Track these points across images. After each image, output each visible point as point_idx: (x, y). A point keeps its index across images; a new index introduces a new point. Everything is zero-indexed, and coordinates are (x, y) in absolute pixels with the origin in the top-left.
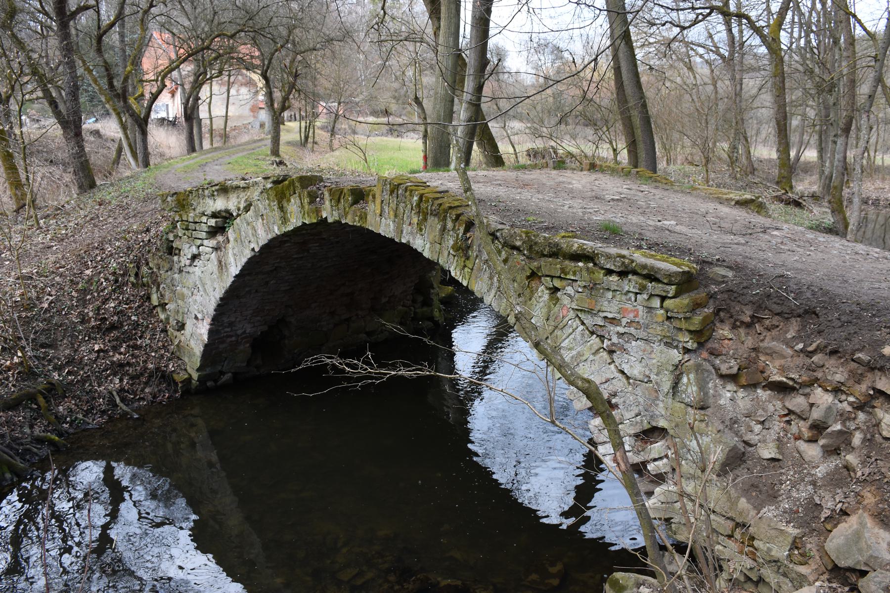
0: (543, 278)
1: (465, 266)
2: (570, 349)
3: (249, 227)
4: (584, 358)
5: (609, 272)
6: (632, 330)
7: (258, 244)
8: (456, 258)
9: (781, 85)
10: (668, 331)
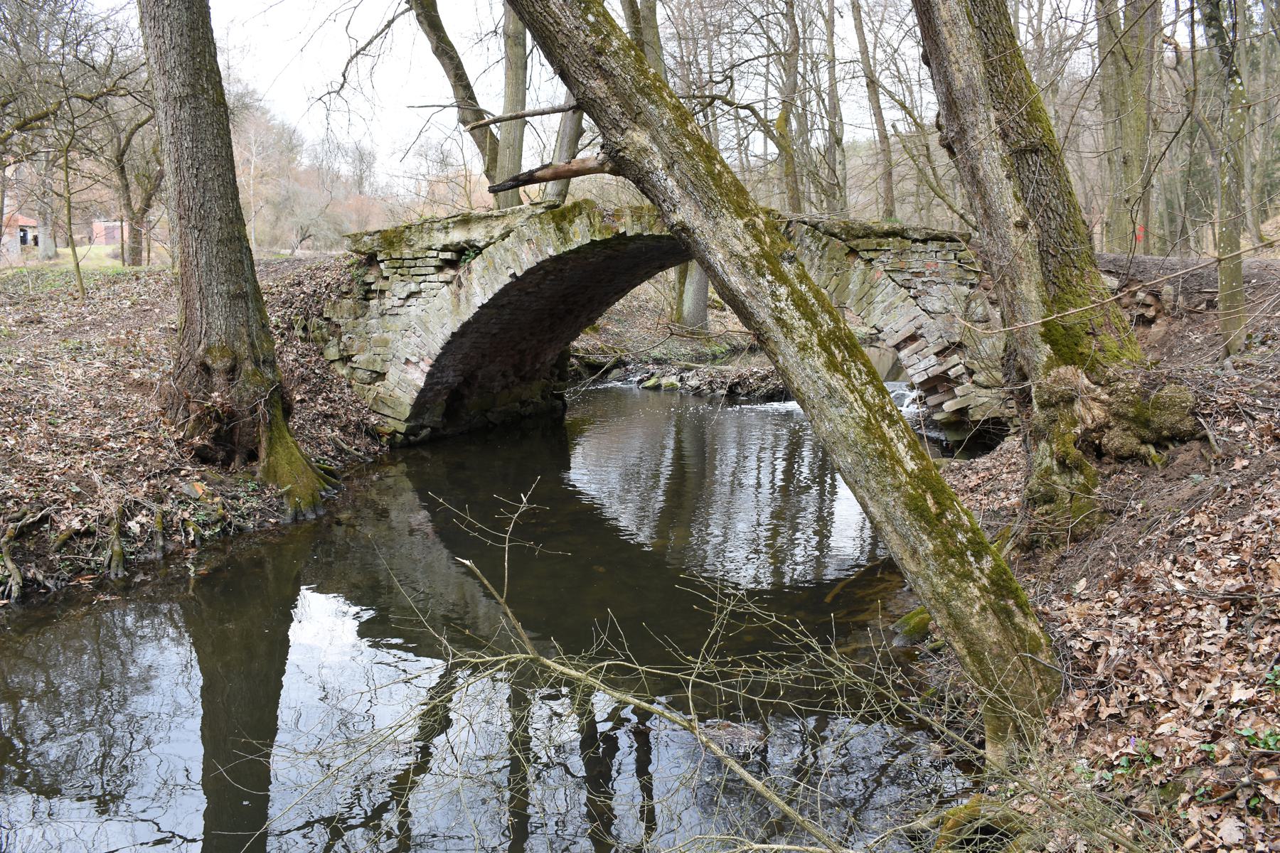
3: (508, 254)
5: (915, 241)
6: (934, 278)
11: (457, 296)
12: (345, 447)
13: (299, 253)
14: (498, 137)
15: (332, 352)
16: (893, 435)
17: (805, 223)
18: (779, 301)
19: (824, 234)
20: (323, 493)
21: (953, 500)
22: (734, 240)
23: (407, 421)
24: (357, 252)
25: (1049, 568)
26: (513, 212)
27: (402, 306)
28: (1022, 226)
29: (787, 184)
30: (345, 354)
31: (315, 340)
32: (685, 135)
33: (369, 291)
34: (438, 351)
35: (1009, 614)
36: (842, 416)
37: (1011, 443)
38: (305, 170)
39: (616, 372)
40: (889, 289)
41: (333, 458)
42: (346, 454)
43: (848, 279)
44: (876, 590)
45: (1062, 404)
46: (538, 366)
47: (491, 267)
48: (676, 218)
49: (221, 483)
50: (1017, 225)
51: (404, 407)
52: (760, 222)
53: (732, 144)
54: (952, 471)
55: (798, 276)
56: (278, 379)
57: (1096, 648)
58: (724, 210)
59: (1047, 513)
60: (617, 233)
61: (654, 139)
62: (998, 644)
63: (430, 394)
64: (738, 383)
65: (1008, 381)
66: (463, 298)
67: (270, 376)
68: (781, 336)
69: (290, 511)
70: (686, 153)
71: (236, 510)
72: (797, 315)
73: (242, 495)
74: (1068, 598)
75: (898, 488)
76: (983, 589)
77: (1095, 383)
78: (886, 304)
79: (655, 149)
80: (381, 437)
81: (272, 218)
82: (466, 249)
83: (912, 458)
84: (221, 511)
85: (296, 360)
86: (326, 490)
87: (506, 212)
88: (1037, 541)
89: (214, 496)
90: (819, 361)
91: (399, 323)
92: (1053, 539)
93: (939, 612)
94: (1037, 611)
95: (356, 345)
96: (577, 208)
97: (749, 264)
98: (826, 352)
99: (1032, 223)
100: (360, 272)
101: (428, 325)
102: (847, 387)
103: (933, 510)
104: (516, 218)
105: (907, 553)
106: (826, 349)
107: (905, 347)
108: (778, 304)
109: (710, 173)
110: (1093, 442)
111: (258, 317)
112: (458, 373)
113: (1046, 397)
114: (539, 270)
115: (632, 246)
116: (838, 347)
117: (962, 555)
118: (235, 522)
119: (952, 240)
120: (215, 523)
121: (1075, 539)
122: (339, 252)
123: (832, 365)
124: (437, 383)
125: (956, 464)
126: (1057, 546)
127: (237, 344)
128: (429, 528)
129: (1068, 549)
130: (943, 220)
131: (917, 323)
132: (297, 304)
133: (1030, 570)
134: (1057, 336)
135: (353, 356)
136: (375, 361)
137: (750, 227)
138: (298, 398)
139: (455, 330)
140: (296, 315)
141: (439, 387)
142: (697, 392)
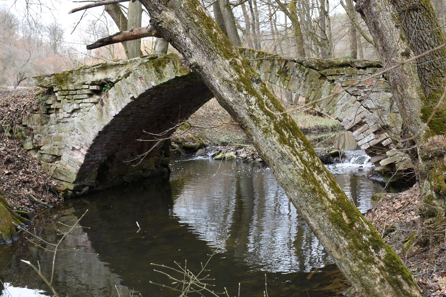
0: (327, 77)
2: (341, 104)
3: (129, 86)
5: (359, 68)
7: (137, 94)
8: (280, 77)
9: (301, 41)
10: (387, 86)
11: (101, 111)
12: (36, 199)
14: (127, 19)
15: (28, 145)
16: (320, 179)
17: (295, 62)
18: (251, 105)
19: (306, 67)
22: (225, 72)
23: (74, 183)
24: (42, 87)
25: (434, 256)
26: (131, 62)
27: (69, 117)
28: (406, 54)
29: (297, 40)
30: (36, 146)
31: (18, 138)
32: (194, 13)
33: (50, 109)
35: (399, 285)
36: (290, 169)
38: (21, 40)
39: (200, 151)
40: (345, 97)
43: (321, 92)
45: (436, 158)
47: (120, 94)
48: (192, 60)
50: (403, 54)
51: (72, 175)
52: (239, 61)
55: (262, 91)
58: (218, 55)
59: (431, 223)
61: (177, 15)
63: (88, 167)
65: (404, 146)
66: (104, 111)
68: (253, 125)
70: (195, 23)
75: (324, 210)
76: (381, 269)
78: (343, 105)
79: (179, 21)
80: (58, 193)
82: (105, 84)
83: (332, 192)
85: (5, 150)
90: (275, 139)
91: (68, 127)
92: (436, 238)
93: (356, 283)
95: (43, 140)
97: (234, 85)
98: (278, 132)
100: (44, 98)
101: (85, 128)
102: (292, 152)
103: (347, 221)
104: (133, 65)
105: (334, 248)
107: (356, 129)
108: (250, 107)
112: (104, 154)
113: (426, 154)
114: (147, 94)
116: (286, 130)
117: (366, 248)
123: (283, 141)
124: (92, 161)
125: (390, 196)
126: (439, 243)
128: (89, 244)
131: (362, 115)
132: (6, 117)
135: (41, 147)
136: (54, 149)
137: (233, 64)
139: (101, 130)
140: (6, 124)
141: (93, 163)
142: (245, 160)
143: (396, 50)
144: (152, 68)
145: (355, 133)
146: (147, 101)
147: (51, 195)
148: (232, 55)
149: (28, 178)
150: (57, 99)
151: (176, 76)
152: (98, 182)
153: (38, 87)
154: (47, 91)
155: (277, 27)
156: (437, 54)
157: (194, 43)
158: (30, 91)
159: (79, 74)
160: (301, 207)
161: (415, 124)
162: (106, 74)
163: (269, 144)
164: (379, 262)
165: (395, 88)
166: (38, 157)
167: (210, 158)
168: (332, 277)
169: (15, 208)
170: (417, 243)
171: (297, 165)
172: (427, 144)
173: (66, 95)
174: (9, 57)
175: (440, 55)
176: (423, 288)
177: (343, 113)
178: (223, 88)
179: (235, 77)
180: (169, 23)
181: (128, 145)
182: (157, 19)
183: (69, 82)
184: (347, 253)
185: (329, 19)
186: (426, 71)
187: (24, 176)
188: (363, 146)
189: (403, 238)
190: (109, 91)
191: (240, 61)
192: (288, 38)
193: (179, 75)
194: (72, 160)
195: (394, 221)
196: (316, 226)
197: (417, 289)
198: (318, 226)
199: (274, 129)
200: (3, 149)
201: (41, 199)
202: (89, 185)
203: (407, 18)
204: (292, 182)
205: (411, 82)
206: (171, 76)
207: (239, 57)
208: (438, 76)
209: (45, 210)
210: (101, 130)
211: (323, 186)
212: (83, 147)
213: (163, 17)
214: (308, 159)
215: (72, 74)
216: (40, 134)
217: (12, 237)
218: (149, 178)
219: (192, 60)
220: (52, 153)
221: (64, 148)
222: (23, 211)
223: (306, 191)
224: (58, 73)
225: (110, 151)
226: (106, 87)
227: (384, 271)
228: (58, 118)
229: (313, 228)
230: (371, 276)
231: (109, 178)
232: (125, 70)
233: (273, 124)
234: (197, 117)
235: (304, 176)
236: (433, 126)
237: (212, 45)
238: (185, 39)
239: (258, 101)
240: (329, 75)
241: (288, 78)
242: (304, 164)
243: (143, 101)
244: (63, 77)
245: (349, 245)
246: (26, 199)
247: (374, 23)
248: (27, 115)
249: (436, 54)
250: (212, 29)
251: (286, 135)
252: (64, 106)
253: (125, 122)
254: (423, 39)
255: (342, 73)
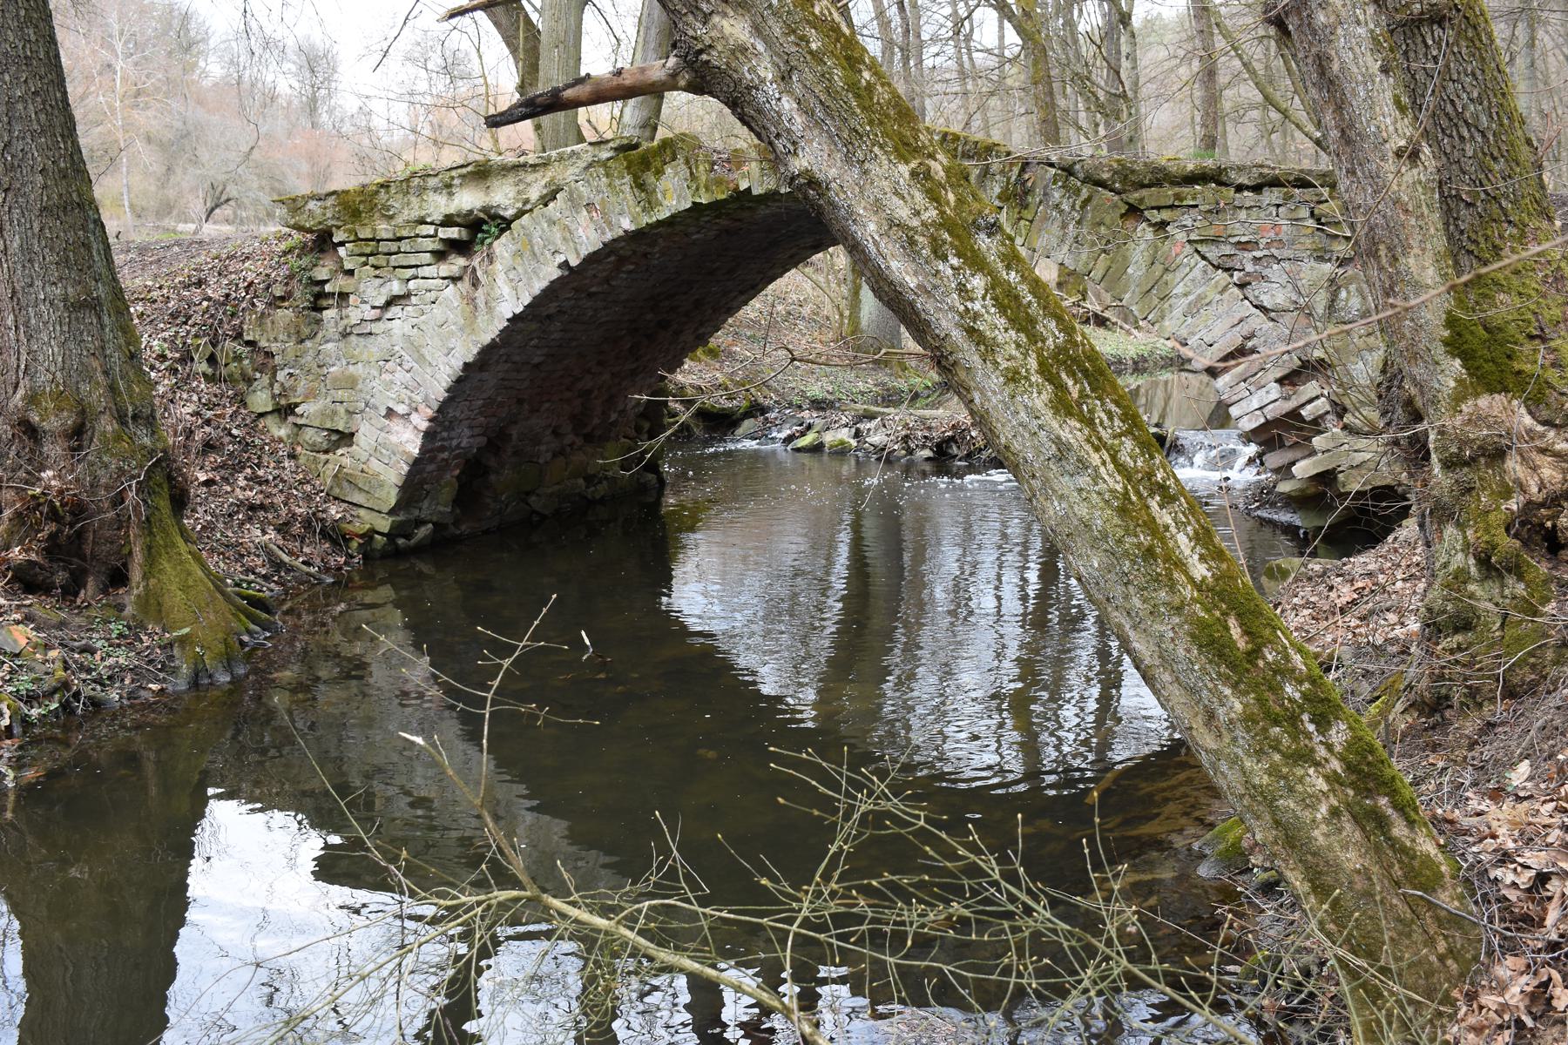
0: (1146, 213)
1: (1020, 219)
2: (1185, 295)
3: (555, 229)
4: (1207, 301)
5: (1240, 188)
7: (578, 254)
9: (1048, 99)
12: (286, 558)
13: (210, 230)
14: (540, 27)
15: (261, 400)
16: (1168, 520)
17: (1052, 165)
18: (972, 300)
19: (1083, 182)
20: (246, 638)
21: (1274, 628)
22: (895, 199)
23: (392, 512)
26: (561, 158)
27: (379, 319)
28: (1411, 155)
29: (1036, 97)
30: (283, 402)
31: (230, 380)
32: (808, 22)
33: (321, 295)
34: (441, 394)
35: (1382, 823)
36: (1081, 490)
37: (1409, 529)
38: (215, 85)
39: (748, 425)
40: (1197, 273)
41: (266, 577)
42: (288, 571)
43: (1125, 258)
44: (1173, 782)
45: (1482, 460)
46: (614, 416)
47: (527, 252)
48: (798, 164)
49: (62, 625)
50: (1399, 154)
51: (386, 490)
52: (938, 168)
53: (943, 31)
54: (1310, 579)
56: (160, 445)
57: (1543, 885)
58: (876, 149)
59: (1459, 649)
60: (736, 190)
61: (757, 30)
62: (1365, 873)
64: (952, 439)
65: (1388, 424)
66: (481, 302)
67: (147, 441)
68: (976, 358)
69: (185, 669)
70: (811, 52)
71: (89, 671)
72: (1001, 322)
73: (99, 644)
74: (1497, 795)
75: (1178, 610)
76: (1333, 779)
77: (1544, 423)
78: (1191, 298)
79: (761, 47)
80: (347, 541)
81: (158, 169)
82: (483, 222)
83: (1202, 558)
84: (61, 673)
85: (197, 414)
86: (249, 632)
87: (549, 157)
88: (1447, 697)
89: (47, 647)
90: (1040, 400)
91: (374, 348)
92: (1473, 692)
93: (1258, 818)
94: (1434, 816)
96: (669, 148)
97: (921, 239)
99: (1427, 150)
100: (305, 262)
101: (424, 351)
102: (1088, 441)
104: (566, 168)
105: (1199, 718)
106: (1052, 379)
108: (969, 305)
109: (853, 87)
110: (1542, 525)
111: (122, 341)
112: (477, 431)
113: (1454, 449)
114: (608, 255)
115: (763, 211)
116: (1072, 374)
117: (1294, 720)
118: (87, 691)
119: (1303, 183)
120: (49, 695)
121: (1511, 693)
122: (273, 228)
123: (1063, 406)
124: (442, 449)
125: (1317, 567)
126: (1480, 705)
127: (85, 388)
129: (1498, 709)
130: (1301, 155)
131: (1245, 329)
132: (197, 318)
133: (1435, 747)
134: (1474, 343)
135: (297, 405)
136: (334, 413)
138: (202, 477)
139: (470, 359)
140: (196, 336)
141: (445, 455)
142: (885, 457)
143: (1381, 140)
144: (623, 178)
145: (1222, 382)
146: (605, 274)
147: (327, 545)
148: (916, 151)
149: (261, 496)
150: (342, 267)
151: (694, 203)
152: (458, 511)
153: (288, 230)
154: (314, 241)
155: (975, 55)
156: (1495, 154)
157: (806, 113)
158: (265, 241)
159: (408, 193)
160: (1108, 599)
161: (1425, 362)
162: (487, 194)
163: (1023, 414)
164: (1326, 760)
165: (1374, 254)
166: (288, 436)
167: (778, 446)
168: (1156, 798)
169: (229, 581)
170: (1411, 706)
171: (1103, 478)
172: (1458, 420)
173: (368, 255)
174: (182, 137)
175: (1503, 156)
176: (1444, 832)
177: (1189, 320)
178: (890, 246)
179: (925, 216)
180: (733, 52)
181: (547, 405)
182: (696, 39)
183: (377, 215)
184: (1240, 733)
185: (1133, 36)
186: (1462, 205)
187: (251, 490)
188: (1246, 418)
189: (1365, 688)
190: (496, 244)
191: (940, 168)
192: (1008, 90)
193: (704, 199)
194: (384, 446)
195: (1335, 641)
196: (1151, 656)
197: (1430, 835)
198: (1156, 656)
199: (1037, 372)
200: (190, 411)
201: (298, 557)
202: (435, 519)
203: (1412, 46)
204: (1086, 526)
205: (1420, 237)
206: (679, 202)
207: (938, 156)
208: (1495, 220)
209: (310, 589)
210: (471, 360)
211: (1176, 542)
212: (416, 410)
213: (714, 34)
214: (1135, 462)
215: (388, 192)
216: (293, 367)
217: (229, 665)
218: (602, 501)
219: (797, 163)
220: (328, 425)
221: (362, 411)
222: (251, 592)
223: (1126, 554)
224: (346, 188)
225: (494, 420)
226: (487, 232)
227: (1341, 784)
228: (345, 322)
229: (1142, 661)
230: (1303, 800)
231: (488, 500)
232: (543, 183)
233: (1034, 356)
234: (768, 330)
235: (1123, 511)
236: (1477, 368)
237: (860, 120)
238: (779, 99)
239: (993, 289)
240: (1153, 208)
241: (1028, 214)
242: (1124, 476)
243: (594, 276)
244: (361, 202)
245: (1244, 712)
246: (258, 556)
247: (1320, 58)
248: (256, 313)
249: (1492, 154)
250: (860, 71)
251: (1071, 390)
252: (362, 285)
253: (538, 338)
254: (1456, 109)
255: (1191, 203)
